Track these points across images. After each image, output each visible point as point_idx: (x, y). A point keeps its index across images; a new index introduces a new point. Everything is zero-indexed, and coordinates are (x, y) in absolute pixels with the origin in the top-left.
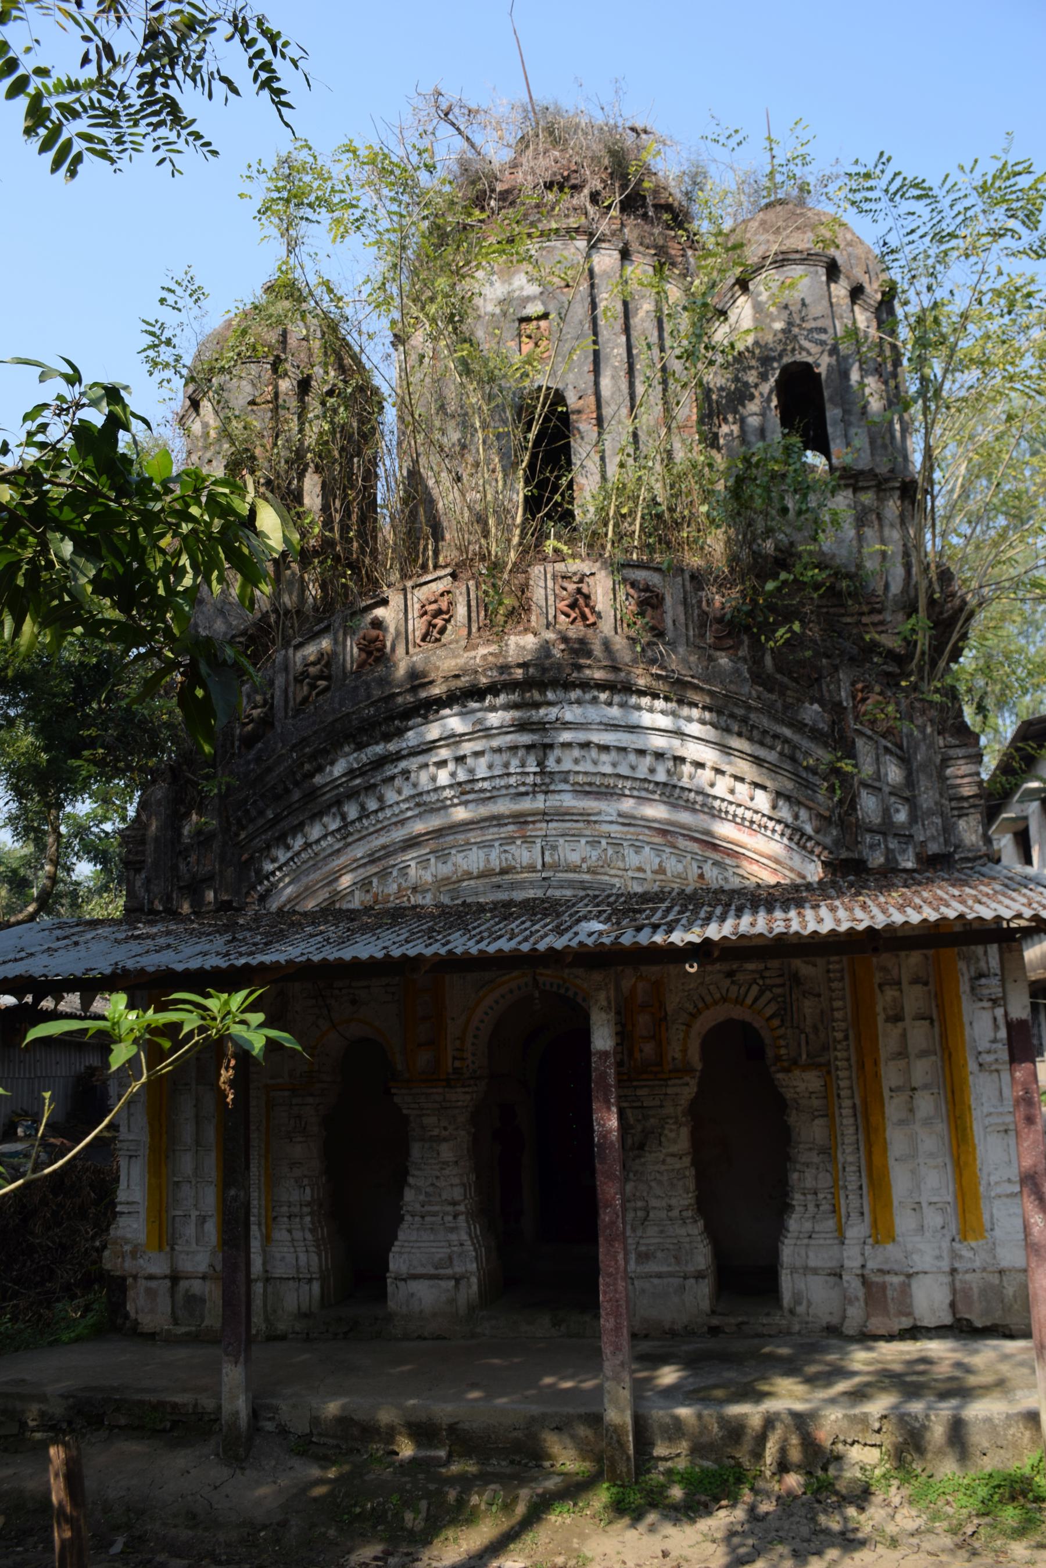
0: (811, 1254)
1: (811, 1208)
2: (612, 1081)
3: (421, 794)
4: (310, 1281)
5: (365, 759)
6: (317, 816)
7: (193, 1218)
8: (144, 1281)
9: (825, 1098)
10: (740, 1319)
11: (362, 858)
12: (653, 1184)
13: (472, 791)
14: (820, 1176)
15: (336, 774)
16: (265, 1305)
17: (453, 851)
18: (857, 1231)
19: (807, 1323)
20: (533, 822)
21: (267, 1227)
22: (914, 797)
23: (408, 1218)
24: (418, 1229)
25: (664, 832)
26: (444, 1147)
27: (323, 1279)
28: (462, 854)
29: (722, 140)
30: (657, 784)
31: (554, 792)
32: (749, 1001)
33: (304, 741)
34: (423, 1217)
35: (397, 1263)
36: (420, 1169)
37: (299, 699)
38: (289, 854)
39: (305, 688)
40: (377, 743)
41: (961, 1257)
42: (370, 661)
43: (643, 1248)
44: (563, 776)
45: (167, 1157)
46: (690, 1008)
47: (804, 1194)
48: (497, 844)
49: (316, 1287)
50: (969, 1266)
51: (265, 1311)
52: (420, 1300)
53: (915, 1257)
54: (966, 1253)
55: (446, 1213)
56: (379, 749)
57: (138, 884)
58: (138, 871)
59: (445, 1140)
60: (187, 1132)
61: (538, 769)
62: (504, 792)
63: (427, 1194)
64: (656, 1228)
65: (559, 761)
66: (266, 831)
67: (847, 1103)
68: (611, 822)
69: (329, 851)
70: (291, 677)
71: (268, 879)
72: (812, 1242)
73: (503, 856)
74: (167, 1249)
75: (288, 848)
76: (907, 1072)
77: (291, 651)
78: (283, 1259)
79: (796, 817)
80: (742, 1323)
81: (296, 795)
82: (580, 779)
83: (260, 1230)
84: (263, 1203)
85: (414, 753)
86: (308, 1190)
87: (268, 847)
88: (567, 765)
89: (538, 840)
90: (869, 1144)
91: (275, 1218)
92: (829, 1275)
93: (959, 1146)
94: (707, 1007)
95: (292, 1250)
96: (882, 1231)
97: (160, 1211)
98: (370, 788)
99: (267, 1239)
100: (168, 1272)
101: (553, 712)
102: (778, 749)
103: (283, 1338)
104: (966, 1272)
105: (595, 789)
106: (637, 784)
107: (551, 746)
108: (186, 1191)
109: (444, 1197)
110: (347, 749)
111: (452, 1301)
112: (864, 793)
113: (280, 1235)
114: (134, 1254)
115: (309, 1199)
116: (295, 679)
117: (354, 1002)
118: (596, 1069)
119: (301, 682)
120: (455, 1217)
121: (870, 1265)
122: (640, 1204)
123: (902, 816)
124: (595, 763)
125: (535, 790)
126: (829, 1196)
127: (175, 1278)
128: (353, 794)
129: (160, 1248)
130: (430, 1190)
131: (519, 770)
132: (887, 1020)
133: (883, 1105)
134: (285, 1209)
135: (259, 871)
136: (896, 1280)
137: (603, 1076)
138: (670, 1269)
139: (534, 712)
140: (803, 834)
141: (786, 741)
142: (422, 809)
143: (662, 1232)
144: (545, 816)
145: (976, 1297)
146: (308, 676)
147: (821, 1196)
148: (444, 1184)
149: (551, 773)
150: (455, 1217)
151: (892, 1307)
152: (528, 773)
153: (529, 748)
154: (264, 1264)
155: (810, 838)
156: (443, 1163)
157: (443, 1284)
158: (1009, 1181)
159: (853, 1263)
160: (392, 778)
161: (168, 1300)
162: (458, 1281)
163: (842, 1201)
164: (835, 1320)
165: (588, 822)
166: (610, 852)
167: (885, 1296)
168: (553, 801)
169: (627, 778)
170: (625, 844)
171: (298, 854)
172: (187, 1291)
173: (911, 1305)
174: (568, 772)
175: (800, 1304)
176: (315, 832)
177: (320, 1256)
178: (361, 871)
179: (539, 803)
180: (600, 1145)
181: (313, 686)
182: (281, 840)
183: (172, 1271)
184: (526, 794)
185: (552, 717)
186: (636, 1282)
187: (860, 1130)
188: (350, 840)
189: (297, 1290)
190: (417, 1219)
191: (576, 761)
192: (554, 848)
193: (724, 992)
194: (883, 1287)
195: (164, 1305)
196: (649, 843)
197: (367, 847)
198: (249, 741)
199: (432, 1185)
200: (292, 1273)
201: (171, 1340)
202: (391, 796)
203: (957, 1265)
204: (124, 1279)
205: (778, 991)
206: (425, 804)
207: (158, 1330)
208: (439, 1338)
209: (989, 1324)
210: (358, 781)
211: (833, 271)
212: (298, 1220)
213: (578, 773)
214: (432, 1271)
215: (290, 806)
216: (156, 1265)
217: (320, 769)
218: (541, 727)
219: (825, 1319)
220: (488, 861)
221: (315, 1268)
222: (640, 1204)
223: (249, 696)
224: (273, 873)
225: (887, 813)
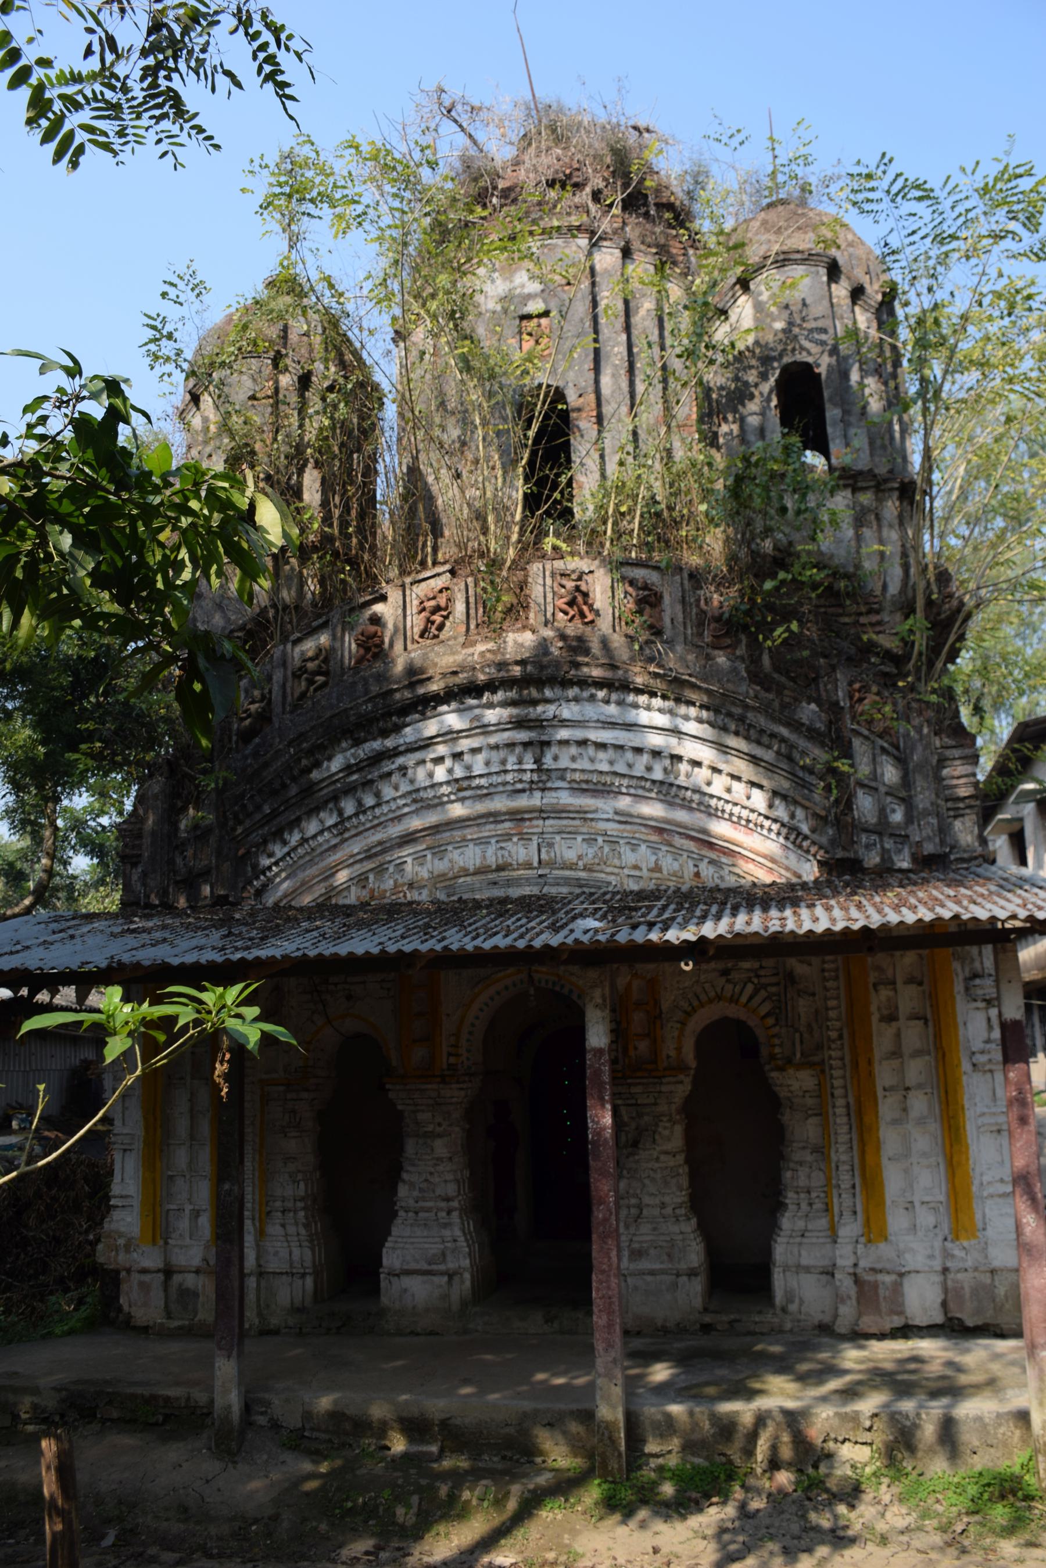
0: (804, 1253)
1: (804, 1206)
2: (606, 1078)
3: (418, 790)
4: (303, 1276)
6: (314, 811)
12: (647, 1182)
13: (469, 788)
16: (258, 1299)
18: (849, 1229)
23: (401, 1213)
25: (660, 831)
27: (316, 1274)
29: (725, 139)
30: (654, 782)
32: (744, 999)
33: (301, 736)
35: (391, 1258)
38: (286, 850)
39: (303, 684)
40: (374, 739)
43: (636, 1246)
49: (309, 1281)
50: (961, 1265)
51: (259, 1306)
56: (376, 745)
57: (135, 877)
58: (134, 865)
60: (182, 1126)
62: (501, 788)
63: (421, 1190)
65: (556, 758)
67: (840, 1102)
74: (161, 1242)
75: (285, 843)
76: (901, 1071)
77: (289, 646)
78: (276, 1254)
79: (792, 816)
81: (294, 790)
82: (577, 776)
85: (412, 749)
86: (302, 1185)
87: (265, 842)
88: (564, 763)
94: (702, 1005)
96: (874, 1230)
99: (261, 1233)
100: (161, 1266)
101: (551, 710)
103: (275, 1332)
104: (959, 1271)
110: (344, 745)
112: (860, 793)
113: (274, 1229)
114: (127, 1248)
116: (294, 674)
117: (349, 997)
120: (449, 1213)
121: (863, 1264)
122: (633, 1201)
123: (897, 817)
124: (592, 760)
125: (532, 787)
127: (168, 1272)
128: (350, 790)
129: (154, 1242)
130: (424, 1185)
133: (876, 1105)
134: (278, 1204)
135: (255, 866)
136: (888, 1279)
137: (598, 1073)
140: (799, 834)
144: (542, 813)
147: (814, 1195)
150: (449, 1213)
151: (884, 1306)
153: (526, 745)
155: (806, 838)
157: (436, 1279)
158: (1002, 1181)
160: (389, 774)
161: (162, 1294)
164: (827, 1319)
166: (606, 849)
167: (877, 1294)
168: (550, 798)
169: (624, 776)
171: (295, 849)
173: (903, 1304)
176: (312, 827)
178: (357, 866)
179: (536, 800)
181: (311, 682)
182: (278, 835)
184: (523, 791)
191: (573, 759)
192: (551, 845)
194: (875, 1286)
195: (157, 1297)
198: (246, 736)
200: (285, 1267)
202: (388, 792)
203: (949, 1264)
204: (117, 1272)
206: (422, 800)
208: (432, 1333)
210: (355, 777)
211: (834, 271)
213: (574, 770)
214: (426, 1267)
216: (150, 1259)
217: (317, 765)
219: (817, 1317)
221: (308, 1263)
222: (633, 1201)
223: (246, 691)
225: (883, 813)
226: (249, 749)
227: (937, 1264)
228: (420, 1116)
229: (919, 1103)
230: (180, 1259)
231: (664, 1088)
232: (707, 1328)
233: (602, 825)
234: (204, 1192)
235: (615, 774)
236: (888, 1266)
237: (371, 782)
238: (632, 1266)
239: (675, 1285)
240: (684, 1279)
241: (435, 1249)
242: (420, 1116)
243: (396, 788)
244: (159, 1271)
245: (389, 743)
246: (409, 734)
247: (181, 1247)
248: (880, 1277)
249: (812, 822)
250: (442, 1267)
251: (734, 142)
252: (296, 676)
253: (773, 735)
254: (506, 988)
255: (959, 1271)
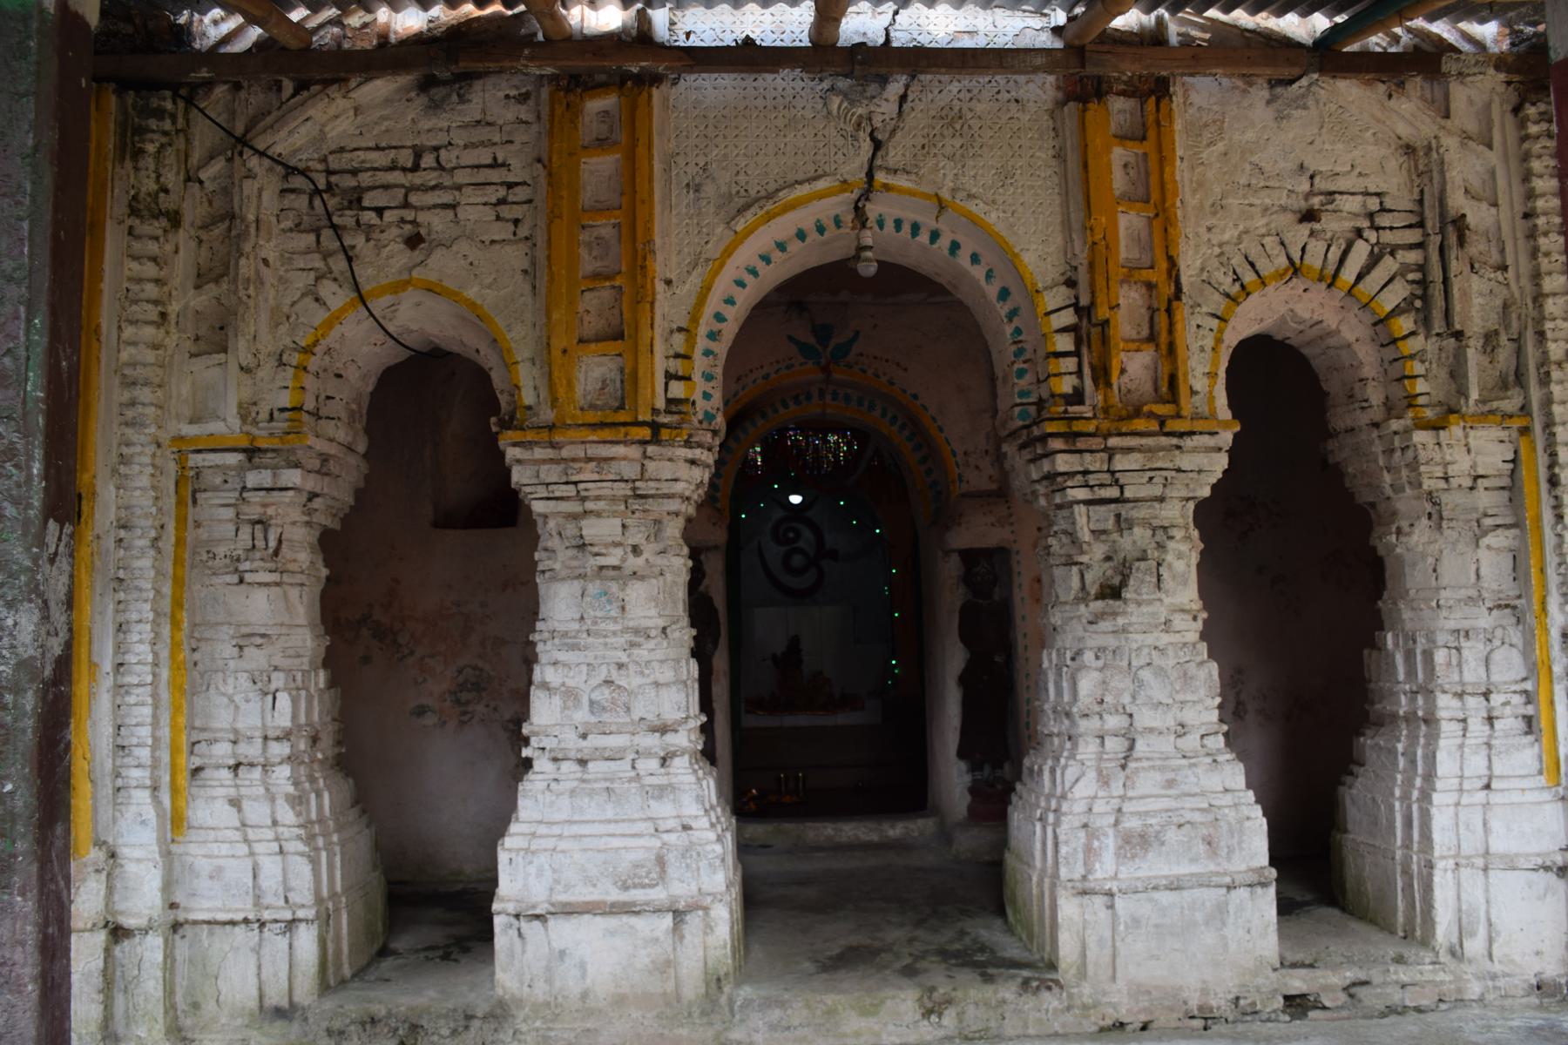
0: (1495, 825)
1: (1477, 726)
4: (292, 924)
9: (1510, 489)
12: (1146, 674)
14: (1497, 656)
16: (169, 991)
19: (1494, 977)
21: (175, 790)
23: (542, 764)
24: (573, 792)
26: (637, 594)
27: (325, 919)
32: (1348, 275)
34: (583, 762)
35: (519, 878)
36: (575, 647)
46: (1227, 283)
47: (1460, 695)
49: (307, 941)
51: (170, 1007)
52: (582, 966)
64: (1158, 777)
72: (1495, 798)
83: (156, 800)
84: (165, 733)
86: (284, 700)
95: (243, 849)
99: (176, 824)
109: (636, 715)
111: (666, 966)
115: (286, 722)
117: (414, 241)
120: (664, 761)
134: (222, 750)
138: (1195, 869)
143: (1170, 783)
147: (1497, 700)
148: (636, 681)
150: (664, 761)
154: (168, 886)
156: (636, 631)
157: (641, 924)
162: (678, 915)
175: (1473, 934)
177: (314, 862)
186: (1119, 902)
189: (257, 950)
190: (567, 767)
199: (608, 682)
200: (242, 907)
205: (1413, 257)
212: (257, 773)
214: (615, 895)
221: (303, 891)
228: (593, 529)
239: (1221, 909)
241: (641, 849)
242: (593, 529)
250: (658, 895)
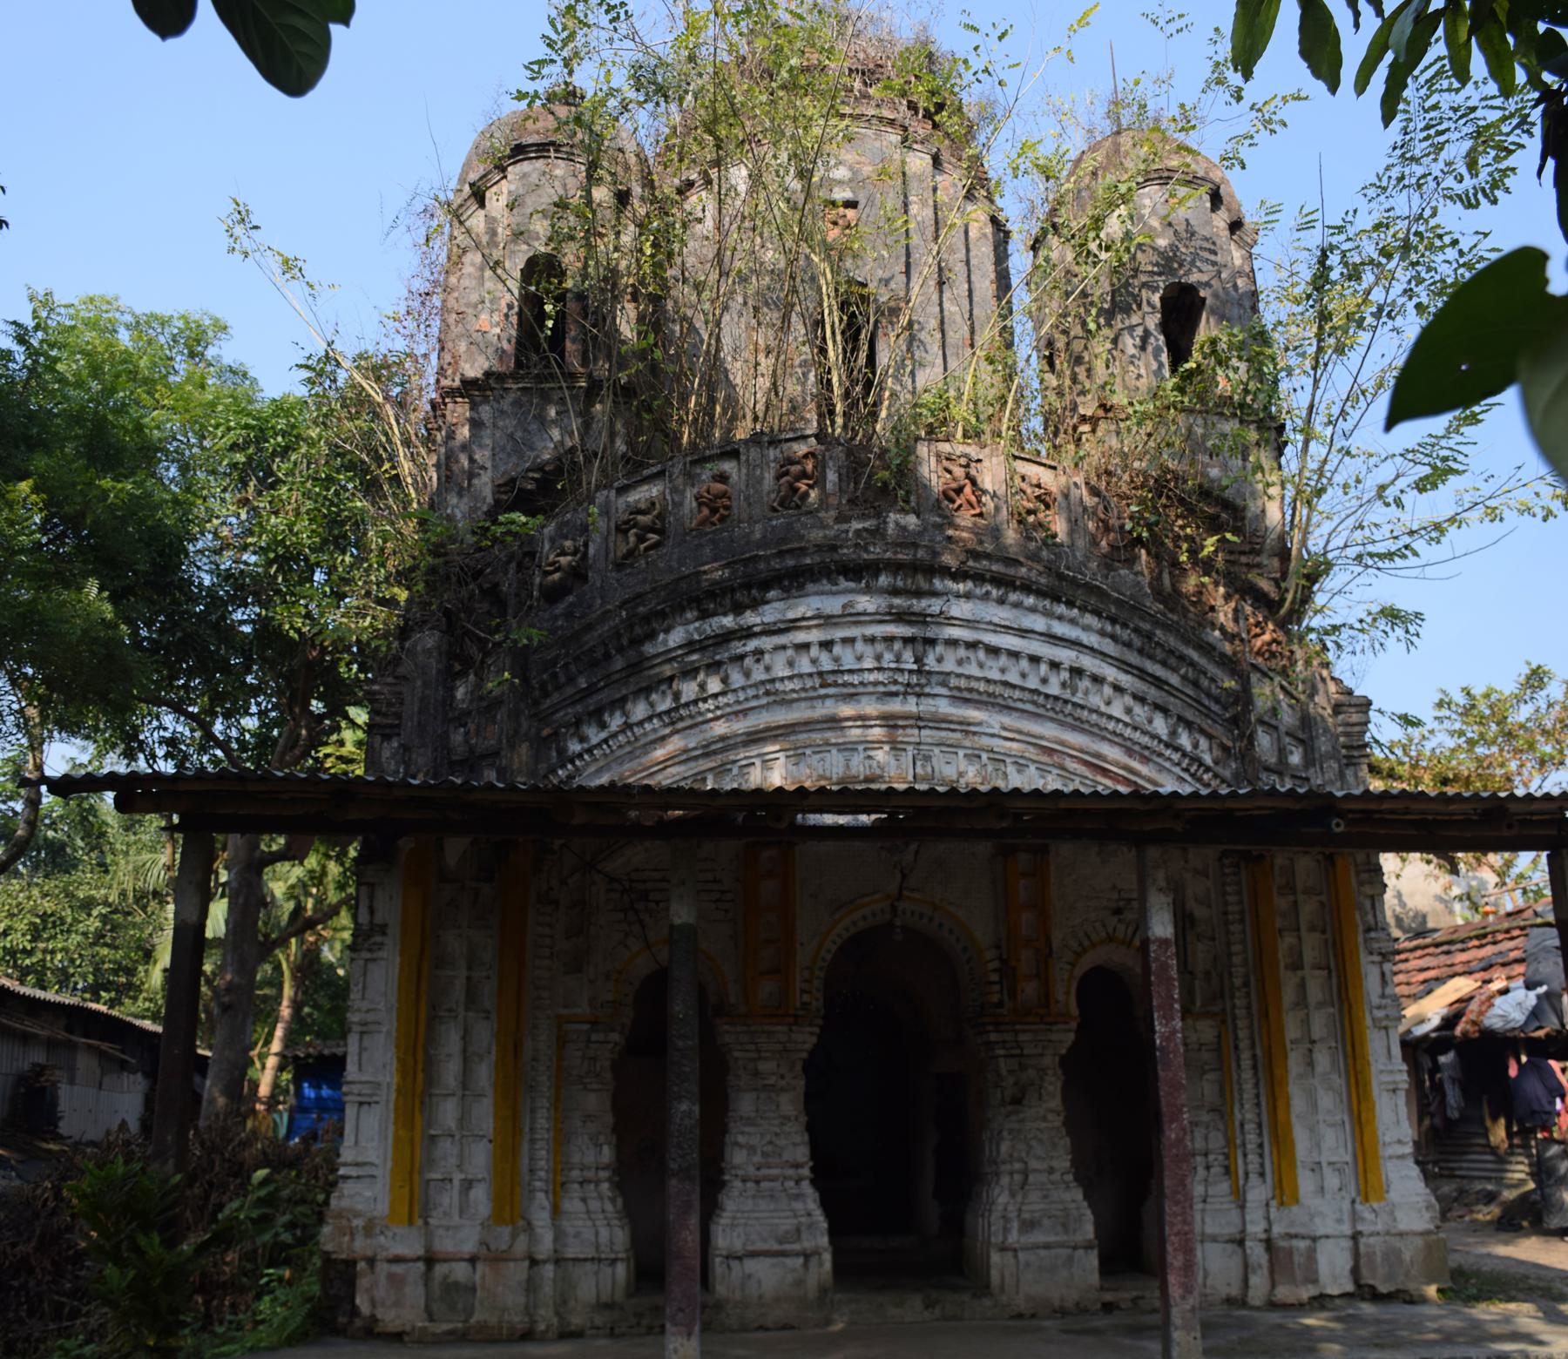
0: (1208, 1220)
2: (1174, 973)
3: (773, 681)
4: (614, 1261)
5: (709, 631)
6: (645, 691)
7: (456, 1183)
8: (386, 1266)
10: (1134, 1294)
11: (695, 749)
12: (1034, 1143)
13: (835, 684)
15: (672, 644)
17: (808, 752)
18: (1257, 1193)
20: (904, 727)
22: (1311, 738)
24: (754, 1197)
25: (1050, 751)
26: (784, 1099)
28: (818, 756)
29: (1162, 23)
30: (1047, 696)
31: (928, 695)
33: (639, 598)
34: (757, 1182)
37: (619, 554)
38: (603, 735)
39: (632, 539)
40: (725, 614)
41: (1363, 1219)
42: (714, 519)
43: (1026, 1216)
44: (941, 678)
45: (422, 1103)
48: (861, 748)
49: (621, 1269)
50: (1372, 1228)
52: (759, 1282)
53: (1317, 1220)
54: (1368, 1216)
55: (786, 1178)
56: (728, 621)
57: (386, 753)
58: (387, 737)
59: (783, 1090)
60: (450, 1072)
61: (915, 667)
62: (870, 689)
63: (764, 1154)
65: (940, 660)
66: (573, 703)
67: (1246, 1057)
68: (993, 735)
69: (652, 737)
70: (613, 525)
71: (572, 762)
73: (867, 762)
74: (420, 1222)
75: (603, 726)
76: (1306, 1022)
77: (613, 493)
78: (577, 1235)
79: (1196, 746)
80: (1138, 1298)
81: (619, 663)
82: (963, 683)
85: (769, 631)
86: (606, 1149)
87: (578, 723)
88: (949, 665)
89: (910, 748)
90: (1273, 1097)
91: (563, 1184)
92: (1227, 1242)
93: (1359, 1103)
94: (1093, 945)
95: (589, 1223)
96: (1284, 1193)
97: (411, 1173)
98: (713, 667)
99: (556, 1211)
100: (421, 1252)
101: (935, 605)
102: (1183, 671)
103: (577, 1335)
104: (1371, 1235)
105: (976, 696)
106: (1027, 696)
107: (932, 642)
108: (446, 1147)
110: (689, 615)
111: (799, 1283)
112: (1260, 730)
113: (572, 1205)
114: (369, 1230)
116: (618, 528)
118: (1157, 959)
119: (626, 532)
120: (798, 1182)
121: (1277, 1230)
122: (1017, 1166)
123: (1295, 758)
124: (981, 665)
125: (908, 690)
126: (1221, 1158)
127: (430, 1260)
128: (689, 673)
129: (411, 1222)
130: (769, 1149)
131: (893, 665)
132: (1286, 968)
133: (1286, 1057)
134: (575, 1174)
135: (562, 751)
136: (1302, 1244)
137: (1165, 967)
138: (1058, 1238)
139: (915, 602)
140: (1201, 764)
141: (1192, 664)
142: (771, 699)
143: (1045, 1197)
144: (919, 721)
145: (1379, 1260)
146: (634, 526)
147: (1211, 1157)
149: (930, 673)
150: (798, 1182)
151: (1299, 1274)
152: (902, 671)
153: (907, 641)
154: (556, 1240)
155: (1208, 769)
157: (789, 1262)
158: (1400, 1142)
159: (1256, 1228)
160: (741, 657)
161: (421, 1290)
163: (1240, 1161)
164: (1235, 1291)
165: (967, 732)
166: (990, 768)
167: (1292, 1262)
168: (927, 706)
169: (1014, 686)
170: (1008, 760)
171: (614, 735)
172: (446, 1277)
173: (1316, 1272)
174: (948, 674)
176: (639, 710)
178: (693, 764)
179: (911, 706)
180: (1162, 1049)
181: (641, 539)
182: (597, 716)
183: (427, 1251)
184: (896, 694)
185: (936, 609)
186: (1021, 1255)
187: (1262, 1084)
188: (680, 725)
189: (597, 1273)
190: (749, 1184)
191: (960, 662)
192: (927, 758)
193: (1110, 931)
194: (1290, 1252)
195: (415, 1294)
196: (1035, 761)
197: (701, 737)
198: (552, 595)
199: (770, 1143)
200: (591, 1253)
201: (427, 1340)
202: (737, 679)
203: (1360, 1228)
204: (351, 1263)
206: (776, 692)
207: (408, 1328)
208: (786, 1327)
209: (1392, 1289)
210: (695, 657)
211: (1216, 199)
212: (592, 1187)
213: (959, 676)
214: (776, 1247)
215: (608, 676)
216: (408, 1244)
217: (652, 636)
218: (922, 619)
219: (1224, 1291)
220: (848, 766)
222: (1017, 1166)
223: (552, 540)
224: (580, 756)
225: (1282, 753)
226: (560, 608)
227: (1347, 1229)
229: (1322, 1060)
230: (444, 1244)
231: (1054, 1037)
232: (1108, 1307)
233: (986, 741)
234: (480, 1157)
235: (1006, 684)
236: (1302, 1231)
237: (719, 664)
238: (1023, 1239)
239: (1070, 1260)
240: (1081, 1252)
241: (788, 1224)
243: (747, 674)
244: (418, 1259)
245: (751, 618)
246: (770, 613)
247: (448, 1228)
248: (1295, 1242)
249: (1217, 753)
250: (797, 1247)
251: (1172, 28)
252: (622, 529)
253: (1182, 658)
254: (864, 918)
255: (1371, 1235)
